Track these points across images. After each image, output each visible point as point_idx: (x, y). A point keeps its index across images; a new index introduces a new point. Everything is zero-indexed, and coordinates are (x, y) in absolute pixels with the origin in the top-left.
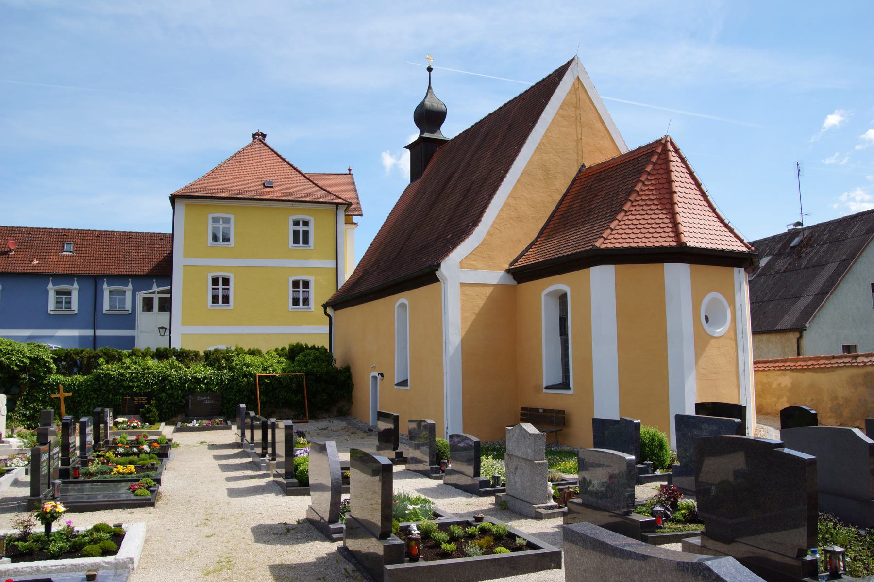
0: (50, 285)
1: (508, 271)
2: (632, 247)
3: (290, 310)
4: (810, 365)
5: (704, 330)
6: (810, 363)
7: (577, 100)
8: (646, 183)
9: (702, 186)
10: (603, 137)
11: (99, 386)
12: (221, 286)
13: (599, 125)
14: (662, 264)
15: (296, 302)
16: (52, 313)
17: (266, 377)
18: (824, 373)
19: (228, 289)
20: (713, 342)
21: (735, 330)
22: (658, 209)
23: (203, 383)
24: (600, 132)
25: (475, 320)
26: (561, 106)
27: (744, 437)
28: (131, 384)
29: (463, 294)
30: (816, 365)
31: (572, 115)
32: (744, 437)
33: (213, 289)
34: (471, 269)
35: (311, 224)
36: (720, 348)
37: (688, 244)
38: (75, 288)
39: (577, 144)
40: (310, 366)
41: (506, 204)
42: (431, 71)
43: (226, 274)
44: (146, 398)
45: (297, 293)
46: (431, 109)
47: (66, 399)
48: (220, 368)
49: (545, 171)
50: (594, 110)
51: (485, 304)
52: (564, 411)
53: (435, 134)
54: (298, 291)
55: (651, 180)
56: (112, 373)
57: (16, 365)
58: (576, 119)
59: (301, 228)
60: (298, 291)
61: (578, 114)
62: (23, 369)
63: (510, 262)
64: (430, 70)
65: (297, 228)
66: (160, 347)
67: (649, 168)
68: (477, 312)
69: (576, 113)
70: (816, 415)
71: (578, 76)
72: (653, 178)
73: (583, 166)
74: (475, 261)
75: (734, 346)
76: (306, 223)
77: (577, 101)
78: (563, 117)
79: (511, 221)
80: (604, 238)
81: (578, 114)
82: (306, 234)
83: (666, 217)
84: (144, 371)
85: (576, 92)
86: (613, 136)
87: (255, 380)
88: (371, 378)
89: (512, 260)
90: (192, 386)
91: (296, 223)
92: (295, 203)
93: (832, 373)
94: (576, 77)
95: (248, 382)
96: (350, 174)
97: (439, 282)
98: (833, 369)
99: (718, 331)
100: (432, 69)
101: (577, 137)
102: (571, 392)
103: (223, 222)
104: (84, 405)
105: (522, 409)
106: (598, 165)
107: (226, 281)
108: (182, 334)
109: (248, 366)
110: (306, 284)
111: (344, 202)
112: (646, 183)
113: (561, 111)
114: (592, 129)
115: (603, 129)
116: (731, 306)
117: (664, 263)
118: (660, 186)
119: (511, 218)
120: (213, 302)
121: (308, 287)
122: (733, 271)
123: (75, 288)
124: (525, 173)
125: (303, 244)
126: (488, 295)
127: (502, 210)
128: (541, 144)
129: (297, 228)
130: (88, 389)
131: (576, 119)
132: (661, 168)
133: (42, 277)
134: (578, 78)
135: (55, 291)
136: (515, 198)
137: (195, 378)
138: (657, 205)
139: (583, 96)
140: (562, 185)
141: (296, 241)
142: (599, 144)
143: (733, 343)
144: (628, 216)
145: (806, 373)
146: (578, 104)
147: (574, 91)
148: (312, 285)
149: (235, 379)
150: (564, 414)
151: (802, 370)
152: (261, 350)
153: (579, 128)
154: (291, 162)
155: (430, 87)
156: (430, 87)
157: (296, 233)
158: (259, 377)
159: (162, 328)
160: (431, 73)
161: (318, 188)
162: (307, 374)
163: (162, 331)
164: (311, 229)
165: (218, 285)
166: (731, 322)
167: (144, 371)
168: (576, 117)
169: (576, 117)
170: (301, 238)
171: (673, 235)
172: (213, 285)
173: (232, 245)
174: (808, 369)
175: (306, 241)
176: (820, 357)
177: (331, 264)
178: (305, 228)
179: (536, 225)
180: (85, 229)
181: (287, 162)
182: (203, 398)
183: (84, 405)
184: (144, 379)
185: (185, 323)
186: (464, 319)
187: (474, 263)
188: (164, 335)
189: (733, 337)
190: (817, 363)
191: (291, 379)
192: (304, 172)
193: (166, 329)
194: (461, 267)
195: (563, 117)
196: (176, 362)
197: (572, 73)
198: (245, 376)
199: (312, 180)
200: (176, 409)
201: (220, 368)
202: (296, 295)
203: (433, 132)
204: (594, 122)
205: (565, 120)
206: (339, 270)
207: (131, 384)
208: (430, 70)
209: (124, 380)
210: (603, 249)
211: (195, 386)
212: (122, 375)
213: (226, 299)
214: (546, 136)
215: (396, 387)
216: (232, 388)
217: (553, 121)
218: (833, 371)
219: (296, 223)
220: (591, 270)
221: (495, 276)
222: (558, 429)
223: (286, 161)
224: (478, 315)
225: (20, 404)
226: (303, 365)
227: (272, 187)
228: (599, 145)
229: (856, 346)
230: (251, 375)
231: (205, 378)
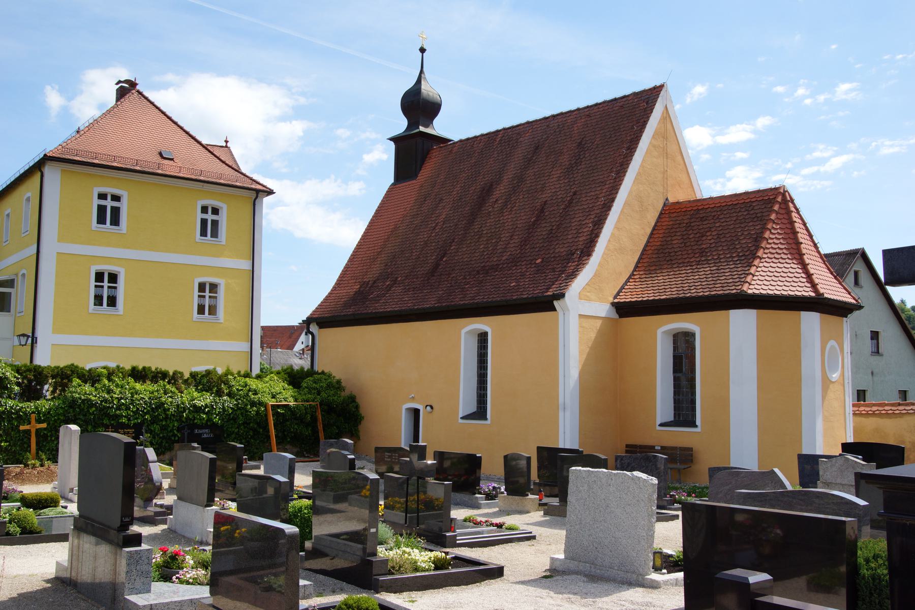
1: (613, 304)
2: (797, 295)
3: (90, 311)
4: (876, 411)
6: (874, 408)
8: (773, 231)
9: (814, 238)
11: (74, 415)
12: (106, 284)
13: (679, 158)
14: (799, 312)
15: (201, 310)
17: (279, 406)
18: (890, 418)
19: (216, 297)
21: (843, 376)
22: (788, 258)
23: (204, 413)
24: (680, 165)
25: (589, 354)
26: (653, 136)
28: (118, 412)
30: (882, 410)
33: (96, 286)
34: (587, 300)
35: (125, 200)
39: (664, 177)
40: (324, 395)
41: (613, 235)
43: (113, 268)
44: (133, 430)
45: (113, 290)
46: (427, 98)
48: (219, 393)
49: (640, 202)
51: (596, 337)
52: (692, 448)
53: (427, 129)
54: (102, 287)
55: (777, 229)
56: (93, 398)
59: (210, 217)
60: (102, 287)
63: (614, 295)
64: (422, 50)
65: (205, 216)
66: (147, 365)
67: (773, 217)
68: (590, 346)
70: (480, 457)
72: (778, 227)
73: (667, 199)
74: (588, 292)
76: (215, 211)
78: (654, 146)
79: (616, 253)
80: (749, 283)
82: (215, 223)
83: (798, 268)
84: (132, 396)
86: (688, 169)
87: (266, 409)
88: (404, 411)
89: (615, 292)
90: (191, 417)
91: (204, 209)
92: (206, 184)
93: (899, 419)
95: (258, 412)
96: (226, 146)
98: (901, 415)
99: (834, 376)
101: (664, 169)
102: (698, 430)
104: (51, 440)
105: (627, 446)
106: (689, 201)
107: (113, 278)
108: (52, 344)
109: (256, 393)
110: (214, 287)
111: (265, 189)
112: (773, 231)
114: (674, 161)
115: (682, 162)
118: (787, 236)
119: (616, 249)
120: (198, 313)
121: (116, 282)
124: (627, 204)
125: (111, 225)
126: (598, 328)
127: (609, 241)
128: (639, 174)
130: (59, 419)
132: (784, 218)
136: (618, 228)
137: (194, 406)
138: (786, 254)
139: (669, 126)
140: (651, 218)
141: (203, 233)
142: (679, 177)
143: (842, 388)
144: (763, 262)
145: (871, 418)
146: (666, 134)
149: (239, 409)
150: (692, 451)
151: (867, 415)
152: (73, 365)
153: (665, 159)
154: (186, 128)
155: (422, 72)
156: (422, 72)
157: (204, 222)
158: (272, 406)
159: (23, 335)
160: (424, 54)
161: (227, 167)
162: (321, 404)
163: (23, 340)
164: (124, 206)
165: (205, 292)
167: (132, 396)
168: (664, 148)
169: (664, 148)
170: (209, 228)
171: (809, 285)
172: (96, 282)
174: (874, 414)
175: (116, 221)
176: (885, 403)
177: (245, 265)
178: (215, 217)
179: (633, 258)
181: (181, 128)
183: (51, 440)
185: (57, 330)
186: (581, 352)
187: (588, 294)
188: (25, 345)
190: (883, 409)
191: (306, 408)
192: (204, 142)
193: (28, 337)
194: (580, 299)
195: (654, 146)
198: (253, 404)
199: (218, 155)
200: (167, 445)
201: (219, 393)
202: (211, 302)
203: (427, 126)
204: (677, 154)
205: (656, 149)
206: (255, 273)
207: (118, 412)
208: (422, 50)
209: (109, 407)
210: (750, 295)
211: (194, 417)
212: (106, 401)
213: (112, 302)
214: (642, 166)
215: (461, 421)
216: (235, 419)
217: (647, 150)
218: (900, 417)
219: (204, 209)
221: (603, 309)
222: (683, 467)
223: (179, 126)
224: (591, 348)
226: (314, 393)
227: (172, 159)
228: (679, 179)
229: (865, 390)
230: (261, 404)
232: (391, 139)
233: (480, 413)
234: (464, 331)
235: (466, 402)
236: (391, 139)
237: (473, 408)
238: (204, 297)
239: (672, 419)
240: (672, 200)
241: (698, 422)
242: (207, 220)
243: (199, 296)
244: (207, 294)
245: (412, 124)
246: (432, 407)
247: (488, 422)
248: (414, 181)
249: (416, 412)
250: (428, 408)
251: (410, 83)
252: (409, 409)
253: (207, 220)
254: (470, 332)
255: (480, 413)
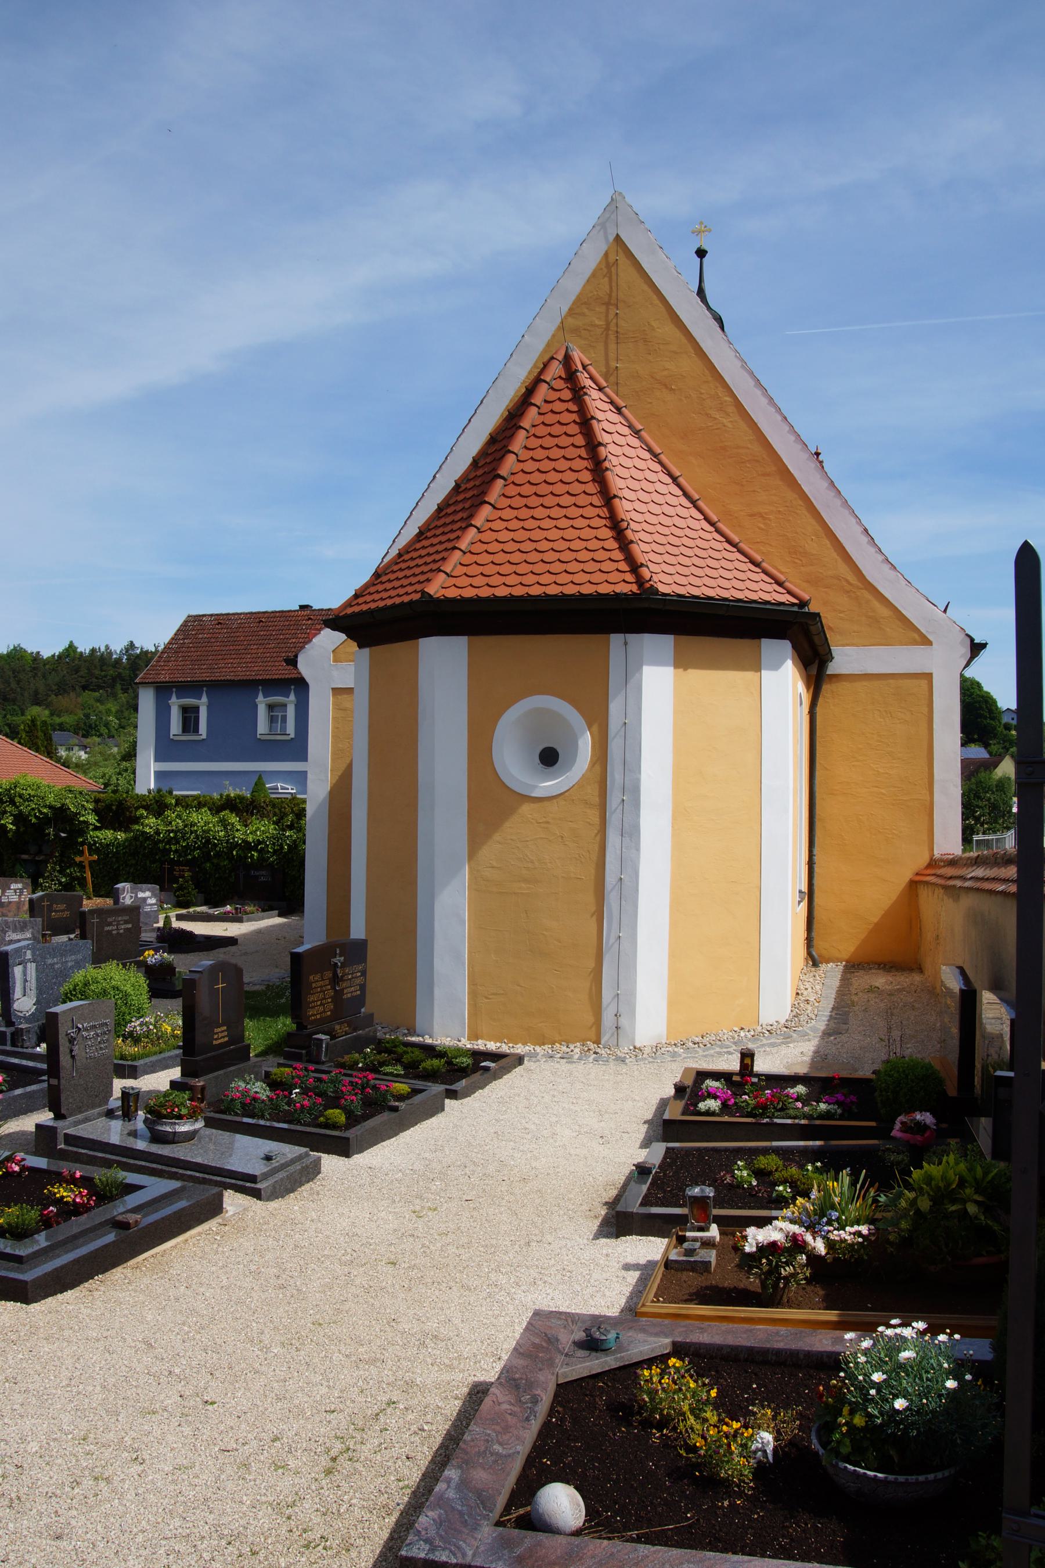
0: (260, 698)
5: (503, 783)
7: (611, 288)
10: (675, 353)
16: (176, 738)
20: (526, 809)
23: (256, 850)
26: (570, 309)
29: (338, 707)
31: (597, 322)
36: (548, 823)
38: (203, 703)
42: (704, 256)
47: (91, 863)
50: (657, 302)
57: (36, 817)
58: (607, 329)
61: (611, 316)
62: (45, 821)
64: (701, 253)
69: (607, 316)
71: (617, 235)
75: (596, 820)
77: (611, 288)
81: (611, 316)
85: (610, 272)
94: (611, 238)
100: (706, 252)
113: (570, 320)
114: (645, 341)
116: (595, 728)
117: (418, 638)
122: (759, 647)
123: (203, 703)
131: (607, 329)
133: (250, 686)
134: (618, 238)
135: (179, 706)
139: (626, 273)
146: (614, 294)
147: (605, 270)
160: (705, 260)
166: (593, 764)
168: (608, 324)
169: (608, 324)
180: (325, 608)
182: (257, 874)
184: (184, 840)
189: (596, 800)
196: (1002, 805)
197: (602, 232)
204: (653, 323)
208: (701, 253)
225: (54, 870)
231: (259, 842)
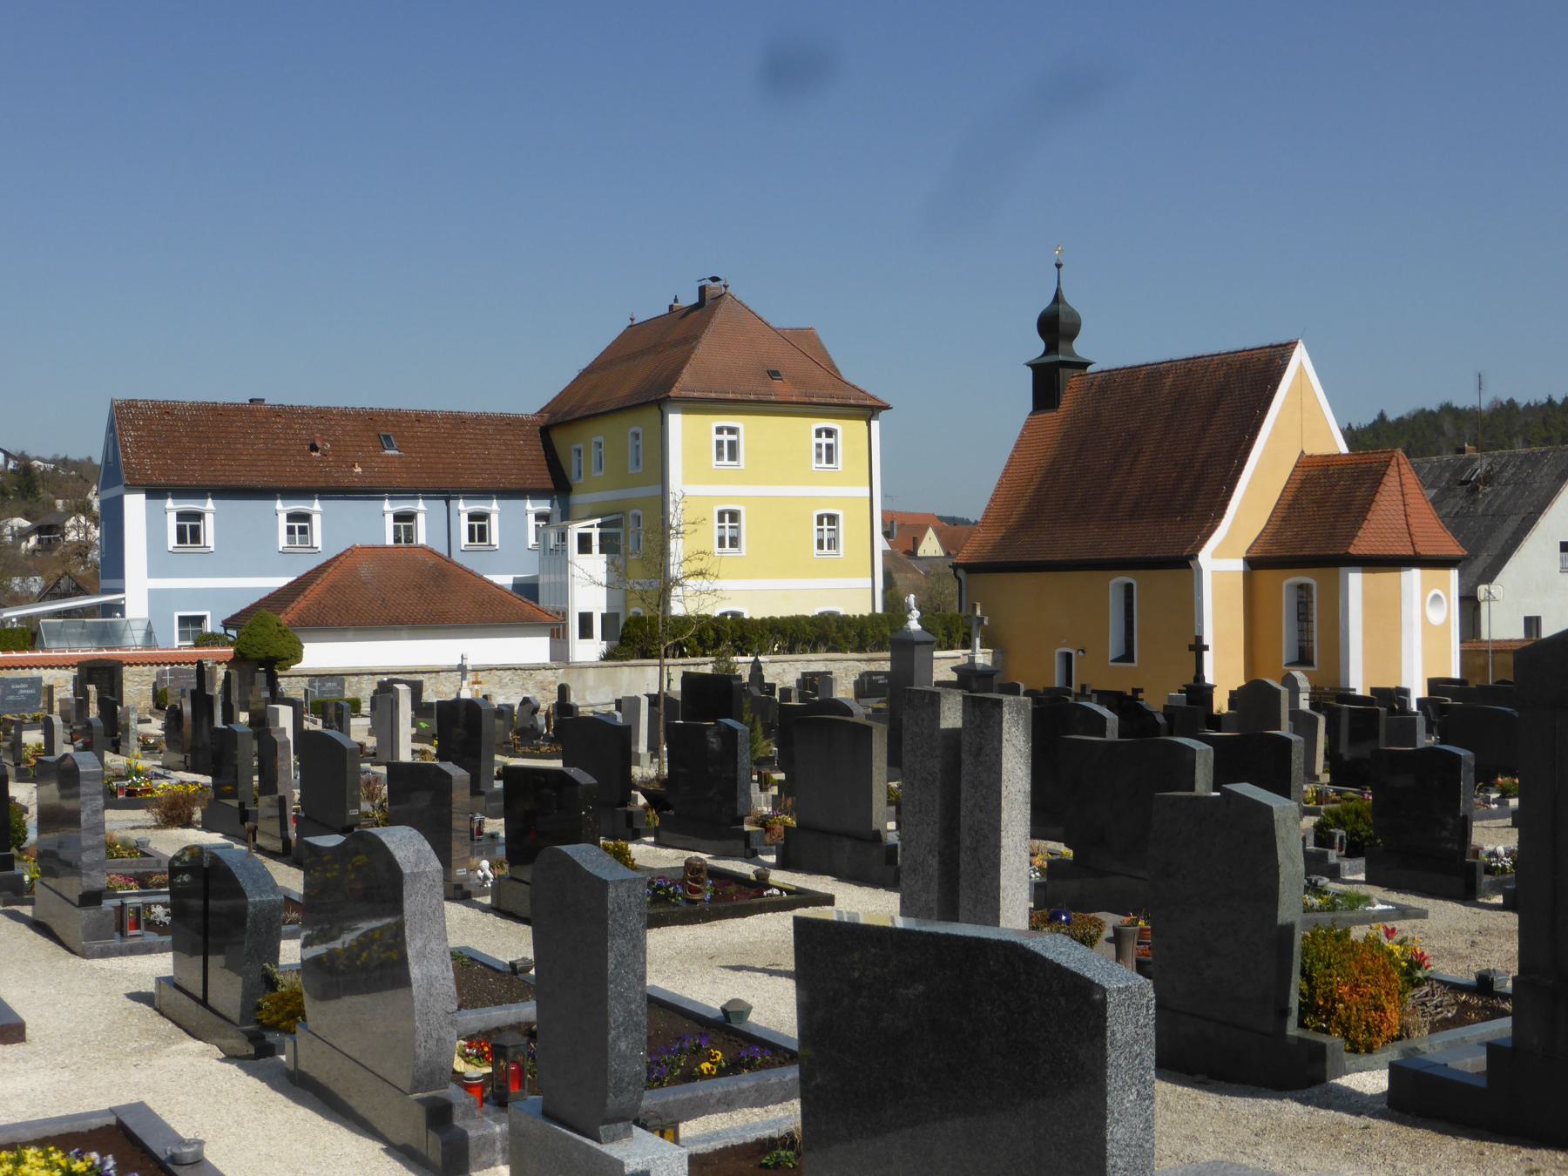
15: (820, 545)
27: (849, 719)
32: (849, 719)
37: (1422, 553)
64: (1058, 266)
65: (720, 437)
73: (1303, 452)
88: (1056, 656)
91: (720, 430)
97: (1187, 570)
103: (728, 434)
129: (720, 437)
141: (720, 455)
148: (743, 518)
157: (720, 444)
173: (742, 467)
208: (1058, 266)
220: (1403, 578)
232: (1029, 365)
233: (1128, 656)
234: (1285, 583)
235: (1115, 646)
236: (1029, 365)
237: (1122, 652)
238: (822, 530)
239: (1297, 659)
240: (1308, 452)
241: (1315, 662)
242: (723, 441)
243: (819, 530)
244: (825, 526)
245: (1051, 348)
246: (1083, 651)
247: (1135, 665)
248: (1055, 414)
249: (1068, 656)
250: (1080, 653)
251: (1045, 302)
252: (1062, 653)
253: (723, 441)
254: (1289, 586)
255: (1128, 656)
